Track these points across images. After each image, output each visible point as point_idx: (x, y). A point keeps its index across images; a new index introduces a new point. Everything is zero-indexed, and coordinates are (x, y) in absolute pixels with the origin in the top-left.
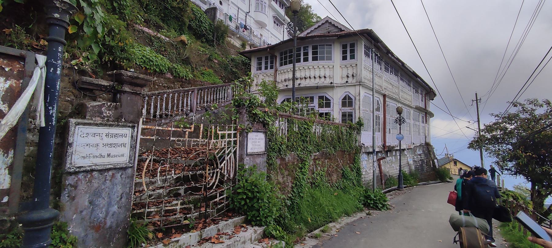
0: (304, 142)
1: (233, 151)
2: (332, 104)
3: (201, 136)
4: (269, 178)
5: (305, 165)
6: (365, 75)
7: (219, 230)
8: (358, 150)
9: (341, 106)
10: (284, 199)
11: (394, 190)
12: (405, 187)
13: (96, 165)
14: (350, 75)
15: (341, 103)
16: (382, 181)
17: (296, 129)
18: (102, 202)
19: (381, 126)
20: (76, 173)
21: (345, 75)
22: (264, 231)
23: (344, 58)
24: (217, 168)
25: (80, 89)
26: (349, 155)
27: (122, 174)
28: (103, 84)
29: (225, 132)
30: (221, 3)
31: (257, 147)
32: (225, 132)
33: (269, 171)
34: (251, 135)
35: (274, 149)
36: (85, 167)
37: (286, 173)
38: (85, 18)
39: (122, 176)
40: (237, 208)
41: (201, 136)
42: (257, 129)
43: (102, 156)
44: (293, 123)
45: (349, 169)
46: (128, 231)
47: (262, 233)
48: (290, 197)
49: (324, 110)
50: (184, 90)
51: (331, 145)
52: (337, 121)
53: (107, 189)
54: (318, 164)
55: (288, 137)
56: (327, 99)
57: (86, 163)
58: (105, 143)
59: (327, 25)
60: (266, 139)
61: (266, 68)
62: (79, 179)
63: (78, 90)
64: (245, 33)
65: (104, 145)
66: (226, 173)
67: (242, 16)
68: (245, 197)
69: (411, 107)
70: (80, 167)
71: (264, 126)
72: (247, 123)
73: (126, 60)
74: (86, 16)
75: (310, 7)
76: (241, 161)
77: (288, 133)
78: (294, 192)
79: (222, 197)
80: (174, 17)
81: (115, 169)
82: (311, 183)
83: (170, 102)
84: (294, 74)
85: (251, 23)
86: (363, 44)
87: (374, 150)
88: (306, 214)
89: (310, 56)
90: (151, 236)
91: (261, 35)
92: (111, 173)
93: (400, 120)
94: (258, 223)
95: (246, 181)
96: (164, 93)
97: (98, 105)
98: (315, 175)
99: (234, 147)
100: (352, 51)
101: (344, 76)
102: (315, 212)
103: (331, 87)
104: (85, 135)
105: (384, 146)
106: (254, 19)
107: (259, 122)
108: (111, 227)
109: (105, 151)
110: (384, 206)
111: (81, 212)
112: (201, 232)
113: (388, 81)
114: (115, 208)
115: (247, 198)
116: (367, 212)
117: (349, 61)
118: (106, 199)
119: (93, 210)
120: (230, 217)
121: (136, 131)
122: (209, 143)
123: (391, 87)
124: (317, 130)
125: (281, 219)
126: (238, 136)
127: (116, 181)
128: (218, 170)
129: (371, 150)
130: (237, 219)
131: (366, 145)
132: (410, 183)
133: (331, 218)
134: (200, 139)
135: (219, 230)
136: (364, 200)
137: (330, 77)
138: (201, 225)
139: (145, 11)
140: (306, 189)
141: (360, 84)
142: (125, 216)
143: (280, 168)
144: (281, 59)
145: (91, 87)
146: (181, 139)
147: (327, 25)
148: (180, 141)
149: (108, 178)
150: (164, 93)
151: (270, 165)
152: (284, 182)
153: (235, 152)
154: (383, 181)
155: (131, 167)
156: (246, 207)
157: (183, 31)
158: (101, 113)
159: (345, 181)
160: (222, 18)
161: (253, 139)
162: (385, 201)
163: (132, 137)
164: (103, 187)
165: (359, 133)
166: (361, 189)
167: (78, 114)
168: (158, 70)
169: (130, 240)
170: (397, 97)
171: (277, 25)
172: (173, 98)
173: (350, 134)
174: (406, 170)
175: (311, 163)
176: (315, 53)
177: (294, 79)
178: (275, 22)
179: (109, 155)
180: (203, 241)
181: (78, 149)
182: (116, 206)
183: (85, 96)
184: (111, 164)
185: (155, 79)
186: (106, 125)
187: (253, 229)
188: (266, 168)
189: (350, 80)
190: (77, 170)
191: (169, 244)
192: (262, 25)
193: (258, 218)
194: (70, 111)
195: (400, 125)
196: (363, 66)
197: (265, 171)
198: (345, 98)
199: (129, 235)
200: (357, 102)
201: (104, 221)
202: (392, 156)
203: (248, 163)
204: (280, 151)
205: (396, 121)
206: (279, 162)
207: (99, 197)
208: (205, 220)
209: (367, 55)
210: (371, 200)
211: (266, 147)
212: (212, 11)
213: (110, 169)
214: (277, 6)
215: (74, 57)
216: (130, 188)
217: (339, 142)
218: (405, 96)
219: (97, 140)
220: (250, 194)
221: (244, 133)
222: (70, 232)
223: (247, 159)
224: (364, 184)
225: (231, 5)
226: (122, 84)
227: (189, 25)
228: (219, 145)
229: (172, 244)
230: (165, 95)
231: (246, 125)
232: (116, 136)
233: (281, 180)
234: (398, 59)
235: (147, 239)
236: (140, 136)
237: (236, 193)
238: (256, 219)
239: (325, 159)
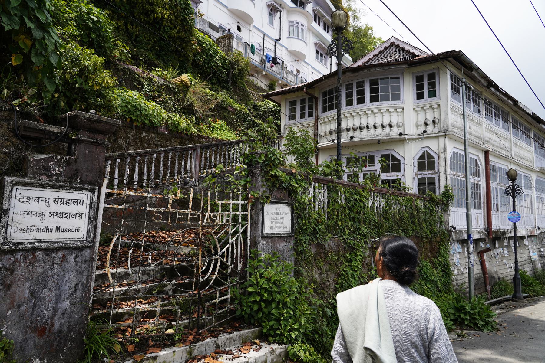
0: (354, 222)
3: (190, 206)
4: (298, 274)
5: (357, 255)
6: (453, 119)
7: (218, 346)
8: (447, 235)
10: (321, 306)
11: (507, 300)
12: (525, 297)
13: (40, 242)
14: (430, 122)
15: (416, 164)
16: (486, 286)
17: (342, 201)
18: (48, 294)
19: (483, 200)
20: (12, 252)
21: (422, 120)
22: (287, 352)
23: (420, 96)
24: (216, 253)
25: (23, 137)
26: (430, 242)
27: (76, 257)
28: (52, 130)
29: (228, 202)
30: (239, 29)
31: (278, 225)
32: (228, 202)
33: (297, 263)
34: (269, 208)
35: (306, 229)
36: (25, 244)
37: (327, 267)
39: (77, 259)
40: (246, 316)
41: (190, 206)
42: (278, 199)
43: (47, 230)
44: (336, 192)
45: (429, 266)
46: (84, 339)
47: (283, 354)
49: (391, 176)
50: (181, 148)
51: (399, 227)
52: (411, 192)
53: (55, 277)
55: (328, 213)
56: (395, 159)
57: (26, 238)
58: (53, 211)
59: (393, 49)
60: (292, 213)
61: (302, 116)
62: (16, 261)
63: (20, 139)
64: (274, 68)
65: (52, 214)
66: (230, 263)
67: (269, 45)
68: (258, 299)
69: (533, 171)
70: (18, 244)
71: (289, 195)
72: (262, 190)
74: (34, 40)
75: (371, 28)
76: (254, 246)
77: (328, 207)
79: (223, 298)
80: (173, 50)
81: (66, 248)
83: (162, 165)
84: (339, 124)
85: (282, 54)
86: (449, 73)
87: (469, 236)
89: (367, 96)
90: (118, 348)
91: (298, 71)
92: (60, 254)
93: (514, 190)
94: (278, 338)
95: (261, 276)
97: (44, 159)
98: (374, 272)
99: (242, 226)
100: (432, 85)
101: (419, 123)
103: (401, 140)
104: (25, 200)
105: (489, 230)
106: (286, 49)
108: (60, 331)
109: (53, 223)
110: (487, 323)
111: (19, 306)
112: (190, 347)
114: (66, 304)
115: (262, 300)
116: (459, 332)
117: (427, 100)
118: (53, 290)
119: (35, 304)
120: (237, 329)
121: (96, 197)
122: (203, 217)
123: (497, 139)
124: (376, 204)
125: (317, 336)
126: (250, 209)
130: (246, 331)
131: (458, 228)
132: (534, 291)
134: (190, 210)
135: (218, 346)
136: (454, 314)
137: (398, 126)
138: (191, 338)
139: (134, 45)
141: (445, 133)
142: (82, 316)
143: (315, 260)
144: (324, 102)
145: (36, 135)
146: (162, 210)
147: (393, 49)
148: (160, 212)
149: (57, 260)
151: (299, 253)
152: (322, 280)
153: (245, 233)
154: (489, 287)
155: (90, 247)
157: (185, 69)
158: (48, 169)
159: (423, 283)
160: (241, 49)
162: (489, 316)
163: (91, 204)
164: (50, 273)
165: (446, 210)
166: (451, 297)
167: (17, 171)
168: (147, 122)
171: (321, 55)
172: (166, 158)
173: (431, 211)
174: (527, 269)
175: (367, 254)
176: (374, 91)
177: (339, 131)
178: (317, 52)
179: (58, 229)
181: (17, 218)
182: (68, 302)
183: (28, 147)
184: (61, 242)
185: (144, 134)
186: (53, 187)
187: (269, 347)
188: (293, 258)
189: (430, 129)
190: (14, 247)
192: (298, 57)
193: (278, 332)
194: (7, 167)
195: (514, 197)
196: (450, 107)
197: (291, 264)
198: (422, 157)
199: (86, 345)
200: (442, 163)
202: (502, 247)
203: (264, 250)
204: (315, 232)
205: (507, 192)
206: (313, 250)
207: (44, 287)
208: (195, 332)
209: (455, 90)
210: (465, 314)
211: (292, 226)
213: (59, 249)
215: (17, 95)
216: (88, 276)
217: (413, 223)
218: (522, 153)
220: (266, 295)
221: (258, 206)
222: (4, 333)
223: (262, 244)
224: (456, 290)
225: (254, 30)
226: (78, 130)
227: (194, 61)
228: (218, 221)
230: (155, 156)
231: (261, 193)
232: (68, 202)
233: (317, 277)
234: (506, 95)
235: (111, 352)
236: (102, 205)
237: (245, 293)
238: (275, 332)
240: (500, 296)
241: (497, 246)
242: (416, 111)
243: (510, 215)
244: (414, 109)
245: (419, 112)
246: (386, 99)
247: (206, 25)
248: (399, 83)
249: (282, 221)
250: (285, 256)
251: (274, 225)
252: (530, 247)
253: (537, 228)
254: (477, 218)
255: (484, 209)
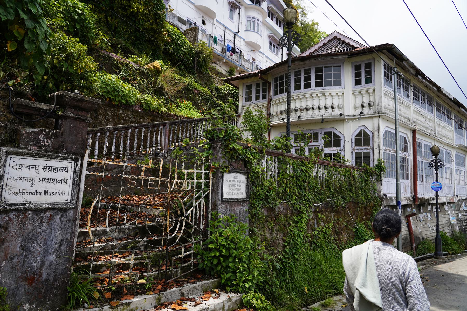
0: (301, 189)
1: (203, 196)
2: (342, 142)
3: (160, 174)
4: (252, 234)
5: (302, 218)
6: (386, 103)
7: (183, 294)
9: (354, 145)
10: (271, 260)
11: (429, 257)
12: (444, 255)
13: (30, 203)
14: (366, 105)
15: (354, 141)
16: (412, 245)
17: (290, 171)
18: (37, 249)
19: (410, 171)
21: (359, 103)
22: (241, 300)
23: (358, 82)
24: (182, 215)
25: (17, 113)
26: (365, 207)
27: (62, 216)
28: (41, 107)
29: (193, 171)
31: (235, 191)
32: (193, 171)
33: (251, 224)
34: (228, 177)
35: (259, 195)
36: (17, 205)
38: (26, 34)
39: (62, 219)
40: (207, 269)
41: (160, 174)
42: (236, 169)
43: (37, 193)
44: (286, 163)
45: (364, 227)
46: (68, 287)
47: (238, 301)
48: (281, 259)
49: (332, 150)
50: (153, 124)
51: (339, 194)
54: (321, 218)
55: (279, 181)
56: (336, 136)
57: (19, 200)
58: (42, 177)
59: (336, 41)
61: (257, 98)
62: (10, 219)
65: (41, 180)
66: (193, 223)
67: (230, 36)
68: (218, 254)
69: (453, 147)
70: (11, 205)
72: (222, 161)
73: (87, 89)
76: (215, 209)
77: (278, 176)
78: (286, 252)
79: (188, 253)
80: (147, 40)
81: (53, 209)
82: (311, 242)
83: (136, 139)
85: (240, 45)
86: (383, 63)
87: (398, 203)
88: (301, 282)
89: (313, 81)
91: (254, 60)
92: (48, 214)
93: (436, 164)
94: (234, 288)
96: (129, 128)
97: (34, 132)
98: (317, 232)
99: (205, 192)
100: (369, 73)
101: (357, 106)
102: (314, 280)
103: (341, 119)
104: (18, 167)
105: (415, 197)
106: (244, 40)
107: (238, 160)
108: (47, 280)
111: (12, 259)
113: (415, 113)
114: (53, 257)
115: (221, 255)
117: (364, 86)
118: (42, 245)
120: (199, 280)
121: (79, 165)
122: (171, 184)
123: (423, 120)
124: (320, 174)
125: (267, 286)
126: (211, 177)
127: (55, 225)
128: (183, 218)
129: (395, 203)
130: (207, 282)
131: (389, 195)
133: (336, 289)
134: (160, 177)
135: (183, 294)
137: (339, 108)
138: (160, 287)
140: (303, 250)
141: (379, 115)
143: (267, 221)
144: (276, 86)
145: (28, 111)
146: (136, 177)
147: (336, 41)
148: (134, 179)
149: (45, 219)
150: (129, 128)
151: (253, 216)
152: (272, 238)
153: (207, 197)
154: (414, 246)
155: (73, 208)
156: (219, 268)
157: (157, 56)
158: (38, 141)
160: (205, 40)
161: (230, 181)
163: (75, 171)
164: (39, 230)
165: (379, 180)
167: (11, 142)
168: (124, 101)
169: (70, 297)
170: (432, 133)
171: (274, 46)
172: (140, 132)
173: (366, 181)
174: (447, 231)
175: (311, 216)
176: (318, 77)
177: (288, 111)
179: (46, 192)
180: (160, 304)
181: (10, 182)
182: (54, 255)
183: (20, 121)
184: (48, 204)
185: (121, 112)
186: (42, 156)
187: (226, 295)
188: (248, 220)
189: (366, 110)
190: (8, 208)
191: (117, 306)
192: (254, 47)
193: (234, 283)
196: (383, 92)
198: (359, 134)
199: (69, 292)
200: (376, 140)
201: (39, 272)
202: (426, 212)
204: (267, 198)
205: (430, 165)
206: (265, 213)
207: (33, 242)
208: (163, 282)
209: (388, 77)
211: (248, 192)
212: (193, 30)
214: (273, 24)
215: (12, 77)
216: (71, 233)
217: (351, 191)
218: (444, 132)
219: (32, 173)
220: (224, 251)
221: (218, 175)
225: (217, 24)
226: (64, 108)
227: (165, 49)
229: (122, 307)
230: (130, 130)
232: (55, 169)
233: (268, 236)
234: (431, 82)
235: (91, 298)
238: (231, 283)
239: (331, 212)
240: (424, 254)
241: (421, 211)
242: (355, 95)
243: (433, 184)
244: (353, 93)
245: (357, 96)
246: (329, 84)
247: (176, 19)
248: (340, 71)
249: (239, 187)
250: (241, 218)
251: (232, 192)
252: (449, 212)
253: (456, 196)
254: (405, 187)
255: (411, 180)
